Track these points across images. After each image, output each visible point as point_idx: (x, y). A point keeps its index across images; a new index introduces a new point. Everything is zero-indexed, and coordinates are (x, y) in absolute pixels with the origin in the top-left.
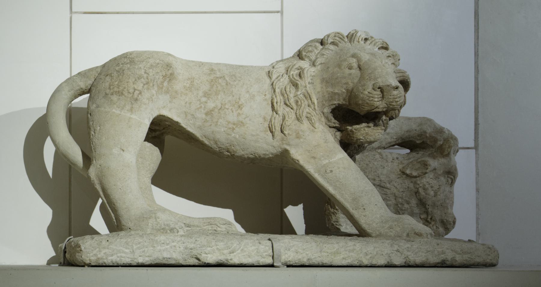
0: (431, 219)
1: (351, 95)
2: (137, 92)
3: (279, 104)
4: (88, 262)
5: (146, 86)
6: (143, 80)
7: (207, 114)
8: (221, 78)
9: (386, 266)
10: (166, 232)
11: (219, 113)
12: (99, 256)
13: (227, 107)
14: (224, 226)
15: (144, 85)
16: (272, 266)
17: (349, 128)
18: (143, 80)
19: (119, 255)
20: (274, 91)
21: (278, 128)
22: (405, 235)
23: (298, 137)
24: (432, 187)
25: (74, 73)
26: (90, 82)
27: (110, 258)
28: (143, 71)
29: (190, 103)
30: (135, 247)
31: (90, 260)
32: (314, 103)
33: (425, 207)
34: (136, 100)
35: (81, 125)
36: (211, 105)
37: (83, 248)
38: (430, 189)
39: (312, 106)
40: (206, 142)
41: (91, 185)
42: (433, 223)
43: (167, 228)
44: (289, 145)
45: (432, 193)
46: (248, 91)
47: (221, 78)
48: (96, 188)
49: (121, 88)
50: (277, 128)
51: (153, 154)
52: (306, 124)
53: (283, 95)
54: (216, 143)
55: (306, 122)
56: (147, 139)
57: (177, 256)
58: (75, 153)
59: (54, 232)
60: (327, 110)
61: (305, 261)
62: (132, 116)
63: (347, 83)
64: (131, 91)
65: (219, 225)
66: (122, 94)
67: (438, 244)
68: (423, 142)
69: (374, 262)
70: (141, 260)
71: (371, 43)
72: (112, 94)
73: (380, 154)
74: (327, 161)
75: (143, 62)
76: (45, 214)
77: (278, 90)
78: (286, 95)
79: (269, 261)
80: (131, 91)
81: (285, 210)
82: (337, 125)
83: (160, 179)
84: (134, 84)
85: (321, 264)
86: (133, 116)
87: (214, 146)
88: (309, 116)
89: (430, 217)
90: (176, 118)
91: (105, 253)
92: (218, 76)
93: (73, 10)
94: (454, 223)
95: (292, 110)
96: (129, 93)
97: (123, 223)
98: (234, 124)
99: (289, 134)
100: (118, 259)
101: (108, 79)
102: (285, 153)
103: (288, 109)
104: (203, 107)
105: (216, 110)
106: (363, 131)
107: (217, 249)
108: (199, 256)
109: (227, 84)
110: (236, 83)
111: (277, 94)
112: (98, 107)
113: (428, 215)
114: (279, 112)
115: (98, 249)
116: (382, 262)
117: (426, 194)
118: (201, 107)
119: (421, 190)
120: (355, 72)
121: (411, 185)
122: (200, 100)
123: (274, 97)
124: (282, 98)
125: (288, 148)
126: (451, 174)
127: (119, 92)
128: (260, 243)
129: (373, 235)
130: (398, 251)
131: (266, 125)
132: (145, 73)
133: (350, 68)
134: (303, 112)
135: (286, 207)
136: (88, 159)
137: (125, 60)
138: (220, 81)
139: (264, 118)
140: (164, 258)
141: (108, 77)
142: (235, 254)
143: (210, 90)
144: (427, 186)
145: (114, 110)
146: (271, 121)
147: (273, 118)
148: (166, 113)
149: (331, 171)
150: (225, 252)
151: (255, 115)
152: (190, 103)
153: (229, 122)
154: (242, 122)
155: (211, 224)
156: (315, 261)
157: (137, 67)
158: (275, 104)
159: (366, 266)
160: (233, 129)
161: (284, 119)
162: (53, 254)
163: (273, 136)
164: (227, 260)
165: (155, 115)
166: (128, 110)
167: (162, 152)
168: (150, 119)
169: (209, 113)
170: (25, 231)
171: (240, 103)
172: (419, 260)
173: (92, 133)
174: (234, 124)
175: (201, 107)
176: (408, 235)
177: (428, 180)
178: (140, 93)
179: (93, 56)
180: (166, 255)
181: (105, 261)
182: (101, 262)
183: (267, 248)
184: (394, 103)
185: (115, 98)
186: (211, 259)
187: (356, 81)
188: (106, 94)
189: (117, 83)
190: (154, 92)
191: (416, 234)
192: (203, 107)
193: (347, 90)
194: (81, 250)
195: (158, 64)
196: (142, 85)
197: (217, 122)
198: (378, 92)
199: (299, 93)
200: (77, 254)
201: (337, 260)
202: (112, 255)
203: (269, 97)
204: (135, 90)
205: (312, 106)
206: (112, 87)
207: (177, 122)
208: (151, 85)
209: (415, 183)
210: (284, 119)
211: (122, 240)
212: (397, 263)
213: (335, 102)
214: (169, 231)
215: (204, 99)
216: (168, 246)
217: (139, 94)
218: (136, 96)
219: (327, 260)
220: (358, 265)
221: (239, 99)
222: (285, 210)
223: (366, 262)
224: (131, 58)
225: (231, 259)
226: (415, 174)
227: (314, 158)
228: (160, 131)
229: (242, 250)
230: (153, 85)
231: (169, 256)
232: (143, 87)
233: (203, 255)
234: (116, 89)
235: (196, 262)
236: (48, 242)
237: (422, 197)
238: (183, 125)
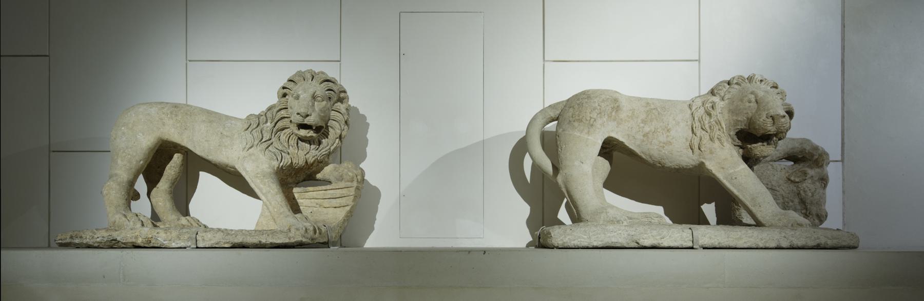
1: (751, 122)
7: (644, 136)
16: (692, 248)
23: (711, 153)
25: (547, 105)
35: (551, 144)
36: (647, 129)
40: (644, 157)
41: (559, 189)
51: (604, 166)
55: (717, 141)
56: (600, 154)
57: (621, 240)
60: (733, 133)
61: (716, 245)
69: (767, 245)
70: (595, 244)
79: (690, 244)
83: (609, 184)
90: (621, 139)
97: (582, 216)
101: (571, 110)
102: (702, 165)
103: (704, 132)
106: (759, 149)
116: (773, 245)
120: (753, 105)
121: (795, 189)
126: (824, 180)
133: (750, 102)
167: (611, 164)
169: (646, 135)
177: (807, 185)
179: (560, 93)
180: (614, 240)
182: (566, 245)
185: (576, 124)
186: (647, 243)
191: (798, 224)
201: (740, 244)
203: (689, 123)
209: (798, 187)
212: (784, 246)
215: (642, 125)
219: (732, 244)
223: (761, 245)
226: (797, 180)
228: (609, 149)
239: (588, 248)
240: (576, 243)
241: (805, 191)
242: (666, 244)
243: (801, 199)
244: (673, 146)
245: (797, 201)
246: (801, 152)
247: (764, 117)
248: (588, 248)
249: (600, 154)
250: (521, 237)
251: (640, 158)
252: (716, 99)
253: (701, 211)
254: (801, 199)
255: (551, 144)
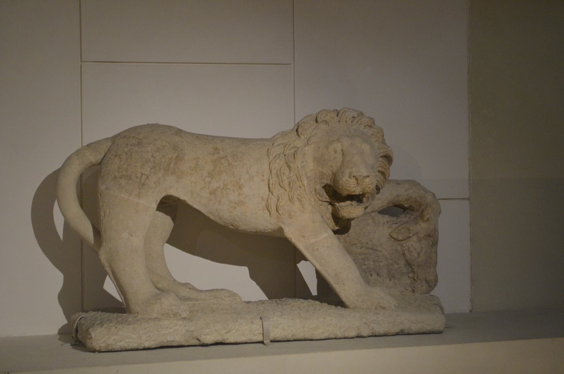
0: (417, 277)
1: (335, 177)
2: (144, 177)
3: (274, 185)
4: (98, 349)
5: (152, 171)
6: (150, 164)
7: (211, 193)
8: (224, 158)
9: (357, 337)
10: (170, 317)
11: (222, 192)
12: (108, 343)
13: (229, 187)
14: (228, 299)
15: (151, 169)
16: (262, 342)
17: (337, 204)
18: (150, 164)
19: (127, 340)
20: (271, 172)
21: (273, 208)
22: (374, 307)
23: (290, 217)
24: (415, 249)
25: (85, 144)
26: (100, 157)
27: (118, 344)
28: (150, 154)
29: (195, 183)
30: (141, 333)
31: (100, 347)
32: (304, 185)
33: (411, 267)
34: (144, 184)
35: (90, 196)
36: (214, 185)
37: (93, 336)
38: (414, 251)
39: (303, 187)
40: (212, 217)
41: (102, 268)
42: (418, 281)
43: (171, 313)
44: (283, 223)
45: (416, 255)
46: (248, 172)
47: (224, 158)
48: (106, 271)
49: (129, 172)
50: (273, 208)
51: (166, 223)
52: (297, 205)
53: (278, 177)
54: (220, 219)
55: (297, 203)
56: (157, 210)
57: (178, 339)
58: (86, 229)
59: (64, 298)
60: (319, 187)
61: (290, 337)
62: (139, 201)
63: (332, 166)
64: (139, 175)
65: (224, 298)
66: (131, 178)
67: (398, 316)
68: (410, 206)
69: (347, 335)
70: (147, 345)
71: (358, 122)
72: (121, 178)
73: (373, 218)
74: (314, 240)
75: (150, 144)
76: (55, 279)
77: (274, 172)
78: (280, 177)
79: (260, 338)
80: (139, 175)
81: (298, 265)
82: (328, 200)
84: (141, 168)
85: (303, 338)
86: (141, 201)
87: (218, 220)
88: (299, 197)
89: (416, 276)
90: (182, 197)
91: (114, 340)
92: (221, 156)
93: (83, 60)
94: (436, 281)
95: (285, 192)
96: (137, 177)
97: (132, 307)
98: (235, 203)
99: (283, 214)
100: (126, 345)
102: (281, 230)
103: (282, 191)
104: (207, 186)
105: (219, 190)
106: (348, 210)
107: (215, 330)
108: (199, 338)
109: (229, 165)
110: (237, 163)
111: (273, 176)
112: (107, 189)
113: (414, 274)
114: (274, 194)
115: (107, 336)
116: (353, 333)
117: (411, 256)
118: (206, 187)
119: (406, 252)
120: (339, 156)
121: (399, 248)
122: (204, 180)
123: (270, 178)
124: (277, 180)
125: (283, 226)
126: (432, 238)
127: (127, 176)
128: (252, 322)
129: (351, 307)
130: (366, 324)
131: (264, 204)
132: (152, 156)
133: (335, 152)
134: (294, 194)
135: (299, 262)
136: (97, 232)
137: (134, 142)
138: (223, 161)
139: (262, 198)
140: (168, 342)
141: (117, 158)
142: (231, 333)
143: (213, 171)
144: (411, 249)
145: (122, 195)
146: (267, 201)
147: (269, 199)
148: (173, 192)
149: (318, 249)
150: (222, 332)
151: (254, 195)
152: (195, 183)
153: (231, 202)
154: (242, 201)
155: (217, 298)
156: (301, 335)
157: (144, 150)
158: (271, 185)
159: (340, 338)
160: (235, 208)
161: (278, 200)
162: (64, 321)
163: (270, 214)
164: (224, 340)
165: (163, 195)
166: (135, 195)
167: (174, 220)
168: (157, 201)
169: (213, 192)
170: (36, 304)
171: (241, 184)
172: (382, 331)
173: (102, 214)
174: (235, 203)
175: (206, 187)
176: (376, 308)
177: (413, 243)
178: (148, 178)
179: (106, 125)
181: (114, 347)
182: (110, 348)
183: (258, 327)
184: (367, 189)
185: (123, 182)
186: (209, 339)
187: (339, 165)
188: (115, 177)
189: (125, 166)
190: (160, 175)
191: (381, 307)
192: (207, 186)
193: (333, 173)
194: (91, 338)
195: (165, 146)
196: (149, 169)
197: (220, 201)
198: (353, 180)
199: (292, 175)
200: (88, 341)
201: (318, 334)
202: (120, 341)
203: (266, 177)
204: (142, 174)
205: (303, 187)
206: (120, 170)
207: (184, 201)
208: (158, 168)
209: (402, 246)
210: (278, 200)
211: (129, 326)
212: (365, 335)
213: (325, 182)
214: (172, 316)
215: (208, 179)
216: (172, 330)
217: (146, 179)
218: (143, 181)
219: (308, 336)
220: (334, 337)
221: (240, 179)
222: (298, 265)
223: (340, 335)
224: (140, 139)
225: (227, 339)
226: (400, 238)
227: (304, 237)
228: (169, 205)
229: (237, 330)
230: (160, 169)
231: (172, 339)
232: (150, 171)
233: (203, 337)
234: (124, 173)
235: (197, 342)
236: (60, 310)
237: (408, 259)
238: (190, 201)
239: (137, 350)
240: (123, 344)
241: (410, 252)
242: (232, 340)
243: (407, 261)
244: (248, 200)
245: (402, 262)
246: (407, 200)
247: (347, 177)
248: (137, 350)
249: (157, 210)
250: (50, 320)
251: (208, 218)
252: (299, 143)
253: (297, 269)
254: (407, 261)
255: (90, 196)
